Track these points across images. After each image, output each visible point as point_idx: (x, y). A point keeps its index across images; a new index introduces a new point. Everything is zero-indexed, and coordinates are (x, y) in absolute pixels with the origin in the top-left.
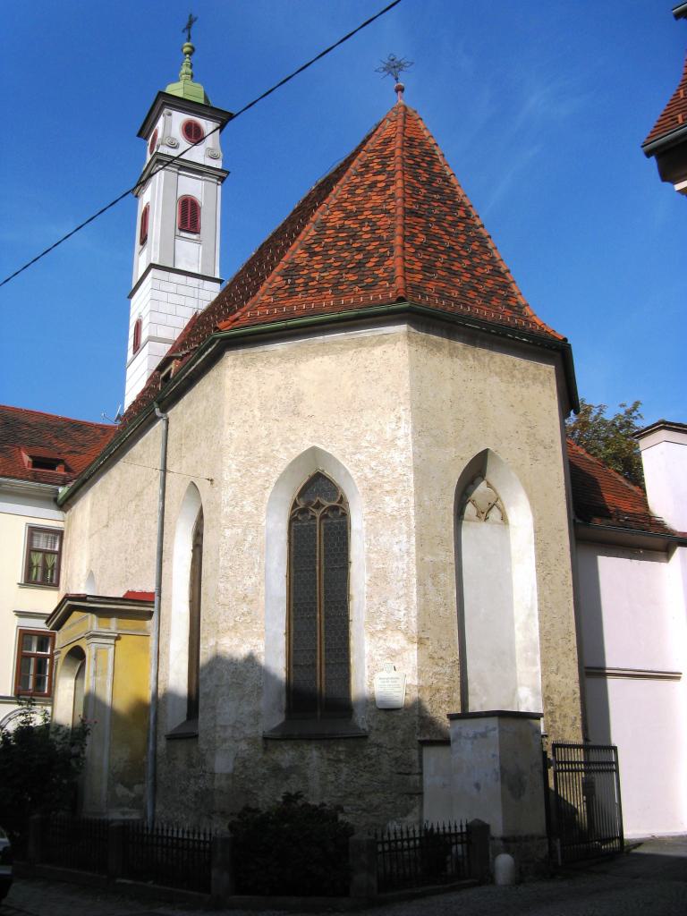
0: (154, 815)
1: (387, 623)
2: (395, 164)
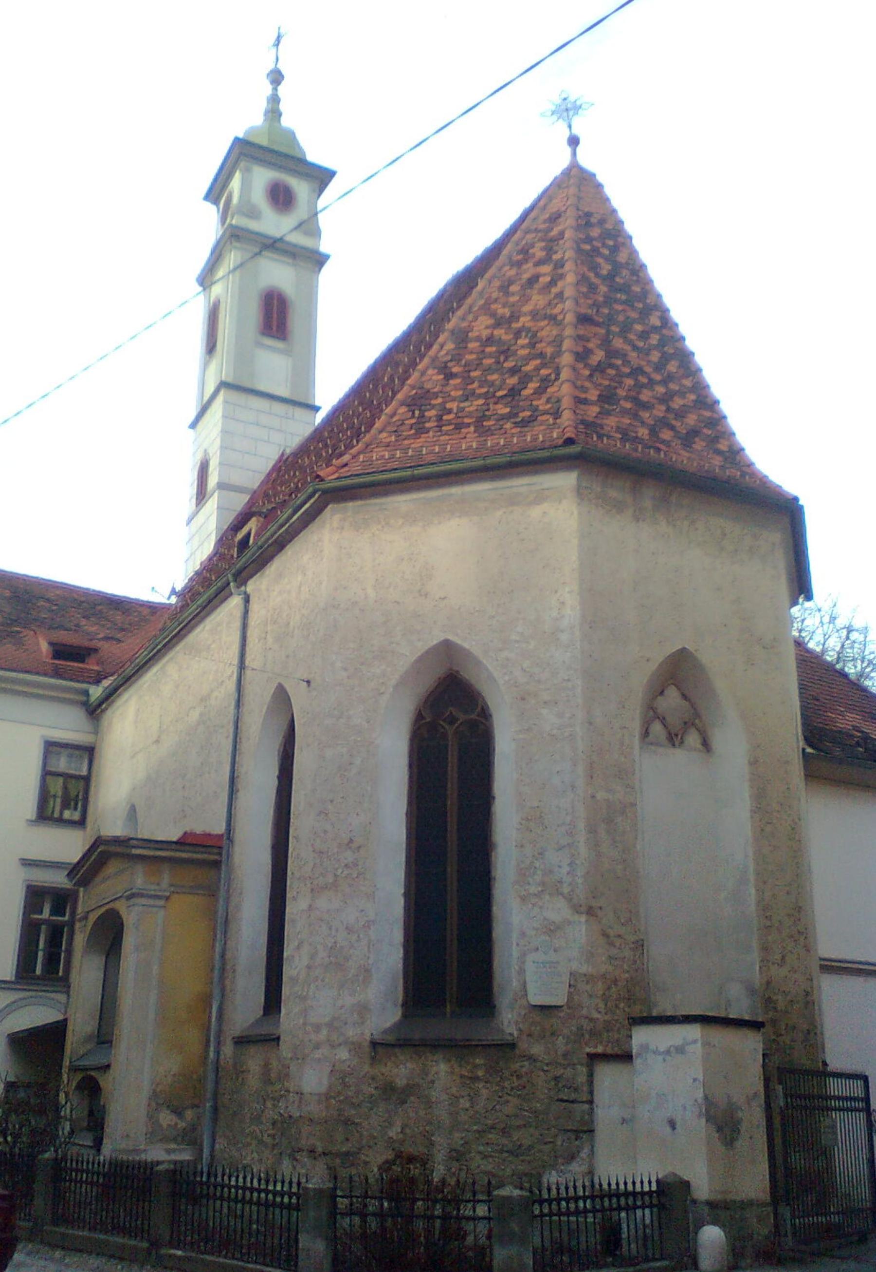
0: (212, 1156)
1: (543, 884)
2: (566, 251)
